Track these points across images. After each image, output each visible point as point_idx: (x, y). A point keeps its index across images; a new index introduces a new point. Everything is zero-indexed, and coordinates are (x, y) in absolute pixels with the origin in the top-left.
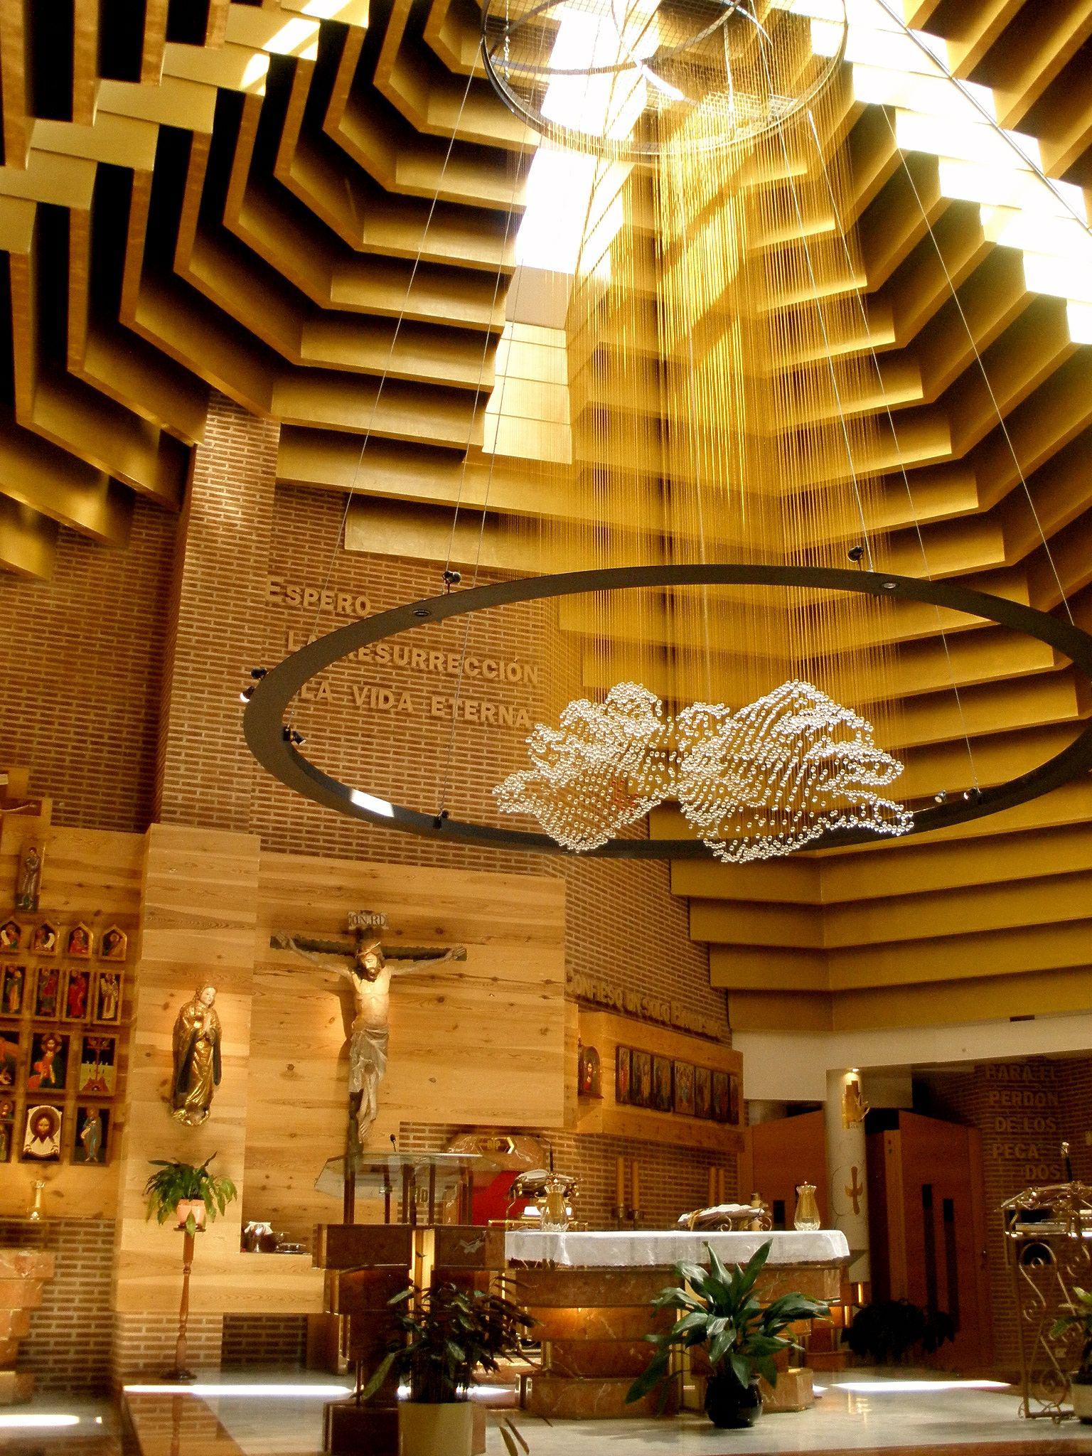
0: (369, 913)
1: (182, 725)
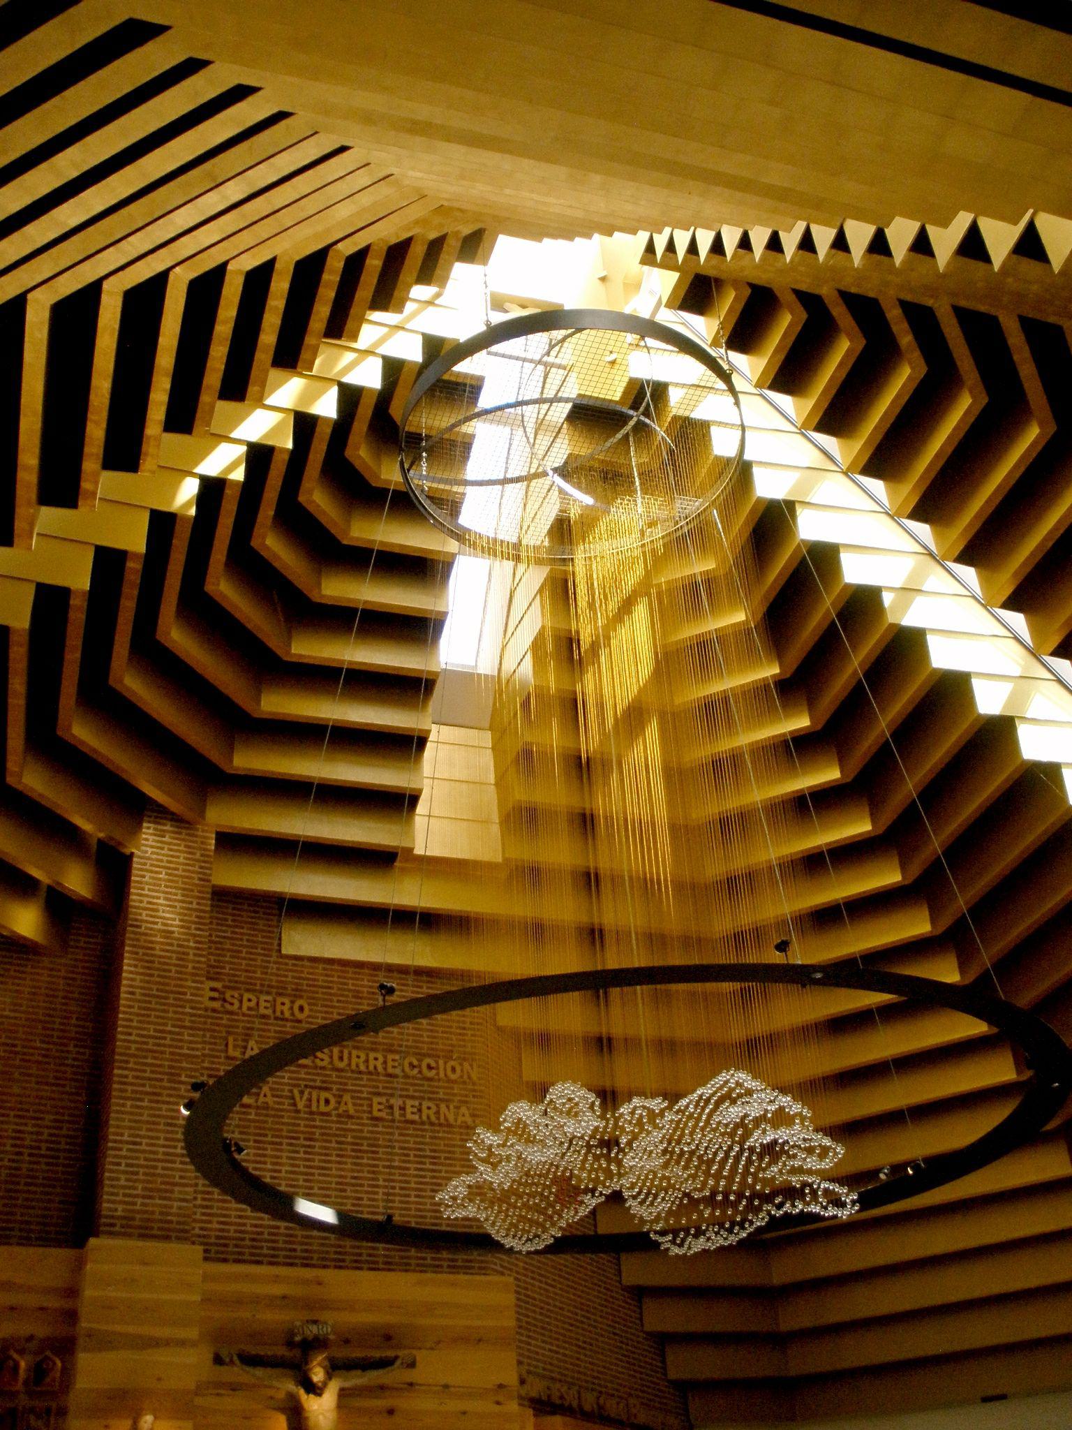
0: (315, 1322)
1: (122, 1135)
